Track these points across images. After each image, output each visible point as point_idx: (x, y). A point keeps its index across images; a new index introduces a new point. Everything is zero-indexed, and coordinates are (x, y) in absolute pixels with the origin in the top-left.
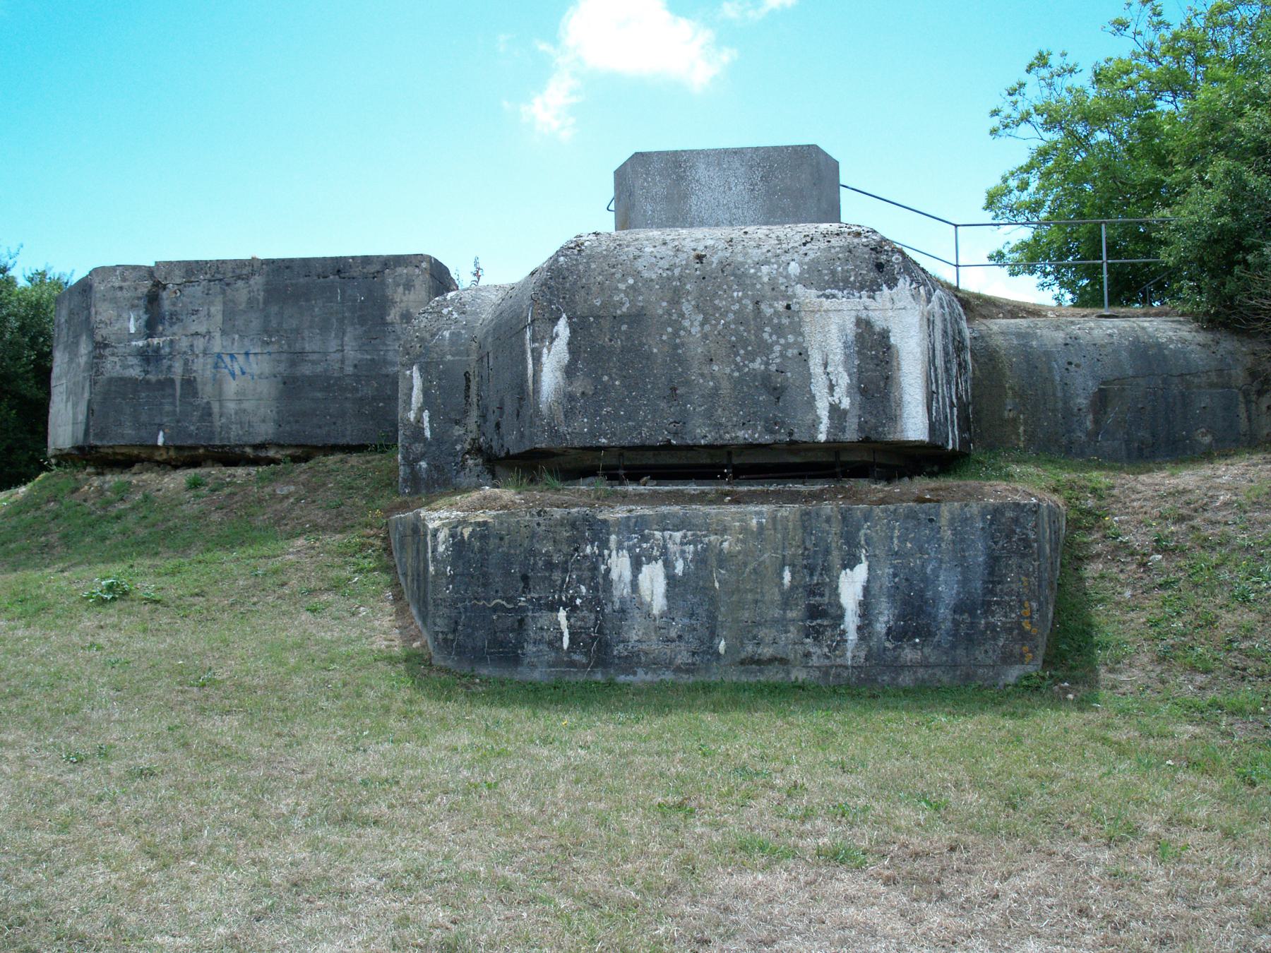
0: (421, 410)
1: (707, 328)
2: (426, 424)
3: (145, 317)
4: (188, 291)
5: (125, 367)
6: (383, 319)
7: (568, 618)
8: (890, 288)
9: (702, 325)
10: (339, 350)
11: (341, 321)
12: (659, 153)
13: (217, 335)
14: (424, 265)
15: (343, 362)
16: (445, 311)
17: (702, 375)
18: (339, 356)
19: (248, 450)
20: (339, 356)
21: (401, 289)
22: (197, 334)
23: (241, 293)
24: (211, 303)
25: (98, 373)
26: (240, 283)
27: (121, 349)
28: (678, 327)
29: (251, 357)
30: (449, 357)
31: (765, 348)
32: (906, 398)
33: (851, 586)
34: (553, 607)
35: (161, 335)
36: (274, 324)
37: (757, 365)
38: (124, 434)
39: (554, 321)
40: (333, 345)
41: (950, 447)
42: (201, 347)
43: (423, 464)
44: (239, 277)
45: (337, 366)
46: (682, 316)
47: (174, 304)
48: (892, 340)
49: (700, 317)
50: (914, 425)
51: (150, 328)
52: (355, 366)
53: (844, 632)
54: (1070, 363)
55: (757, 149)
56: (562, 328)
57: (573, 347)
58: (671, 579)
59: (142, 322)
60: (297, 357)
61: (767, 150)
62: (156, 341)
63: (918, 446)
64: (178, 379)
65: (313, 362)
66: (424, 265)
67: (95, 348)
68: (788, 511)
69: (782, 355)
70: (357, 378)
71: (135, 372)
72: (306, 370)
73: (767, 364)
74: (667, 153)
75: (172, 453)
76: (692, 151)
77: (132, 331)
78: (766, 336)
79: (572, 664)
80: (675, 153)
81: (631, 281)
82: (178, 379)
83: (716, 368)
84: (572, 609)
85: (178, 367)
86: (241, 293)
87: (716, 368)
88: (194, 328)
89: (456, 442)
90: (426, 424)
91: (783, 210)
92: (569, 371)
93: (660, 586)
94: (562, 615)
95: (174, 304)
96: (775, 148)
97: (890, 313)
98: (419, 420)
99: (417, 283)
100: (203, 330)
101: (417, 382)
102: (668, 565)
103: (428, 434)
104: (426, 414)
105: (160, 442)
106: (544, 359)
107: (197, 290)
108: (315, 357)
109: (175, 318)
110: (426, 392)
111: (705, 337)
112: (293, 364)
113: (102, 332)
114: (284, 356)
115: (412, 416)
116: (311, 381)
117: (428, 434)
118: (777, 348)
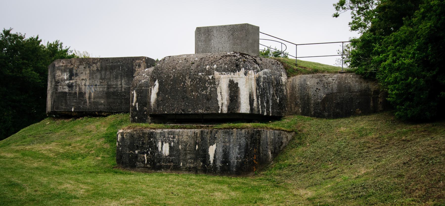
0: (136, 102)
1: (192, 83)
2: (137, 106)
3: (69, 74)
4: (80, 67)
5: (63, 89)
6: (132, 75)
7: (147, 156)
8: (239, 72)
9: (191, 82)
10: (121, 84)
11: (121, 76)
12: (203, 27)
13: (88, 80)
14: (144, 60)
15: (121, 88)
16: (143, 75)
17: (190, 95)
18: (120, 86)
19: (97, 113)
20: (120, 86)
21: (137, 67)
22: (83, 79)
23: (94, 67)
24: (86, 71)
25: (57, 90)
26: (94, 65)
27: (63, 83)
28: (185, 82)
29: (97, 86)
30: (143, 88)
31: (206, 88)
32: (241, 102)
33: (212, 150)
34: (144, 153)
35: (73, 80)
36: (103, 77)
37: (204, 92)
38: (63, 108)
39: (155, 81)
40: (119, 83)
41: (271, 115)
42: (84, 83)
43: (136, 118)
44: (94, 63)
45: (120, 89)
46: (186, 79)
47: (77, 71)
48: (239, 86)
49: (190, 80)
50: (244, 108)
51: (70, 78)
52: (125, 89)
53: (210, 161)
54: (317, 89)
55: (230, 25)
56: (157, 83)
57: (159, 89)
58: (170, 147)
59: (68, 76)
60: (109, 87)
61: (233, 25)
62: (71, 81)
63: (256, 114)
64: (78, 92)
65: (114, 88)
66: (144, 60)
67: (56, 83)
68: (198, 131)
69: (210, 90)
70: (125, 92)
71: (67, 90)
72: (112, 90)
73: (206, 92)
74: (205, 27)
75: (77, 114)
76: (212, 27)
77: (65, 78)
78: (206, 85)
79: (147, 167)
80: (208, 27)
81: (174, 70)
82: (78, 92)
83: (194, 93)
84: (147, 153)
85: (78, 89)
86: (94, 67)
87: (194, 93)
88: (82, 78)
89: (145, 112)
90: (137, 106)
91: (237, 43)
92: (158, 94)
93: (168, 149)
94: (145, 155)
95: (77, 71)
96: (236, 25)
97: (238, 78)
98: (135, 105)
99: (142, 65)
100: (84, 78)
101: (135, 95)
102: (170, 144)
103: (137, 109)
104: (137, 104)
105: (73, 110)
106: (152, 91)
107: (82, 67)
108: (114, 86)
109: (77, 75)
110: (137, 97)
111: (191, 85)
112: (108, 88)
113: (57, 78)
114: (106, 86)
115: (134, 104)
116: (114, 93)
117: (137, 109)
118: (209, 88)
